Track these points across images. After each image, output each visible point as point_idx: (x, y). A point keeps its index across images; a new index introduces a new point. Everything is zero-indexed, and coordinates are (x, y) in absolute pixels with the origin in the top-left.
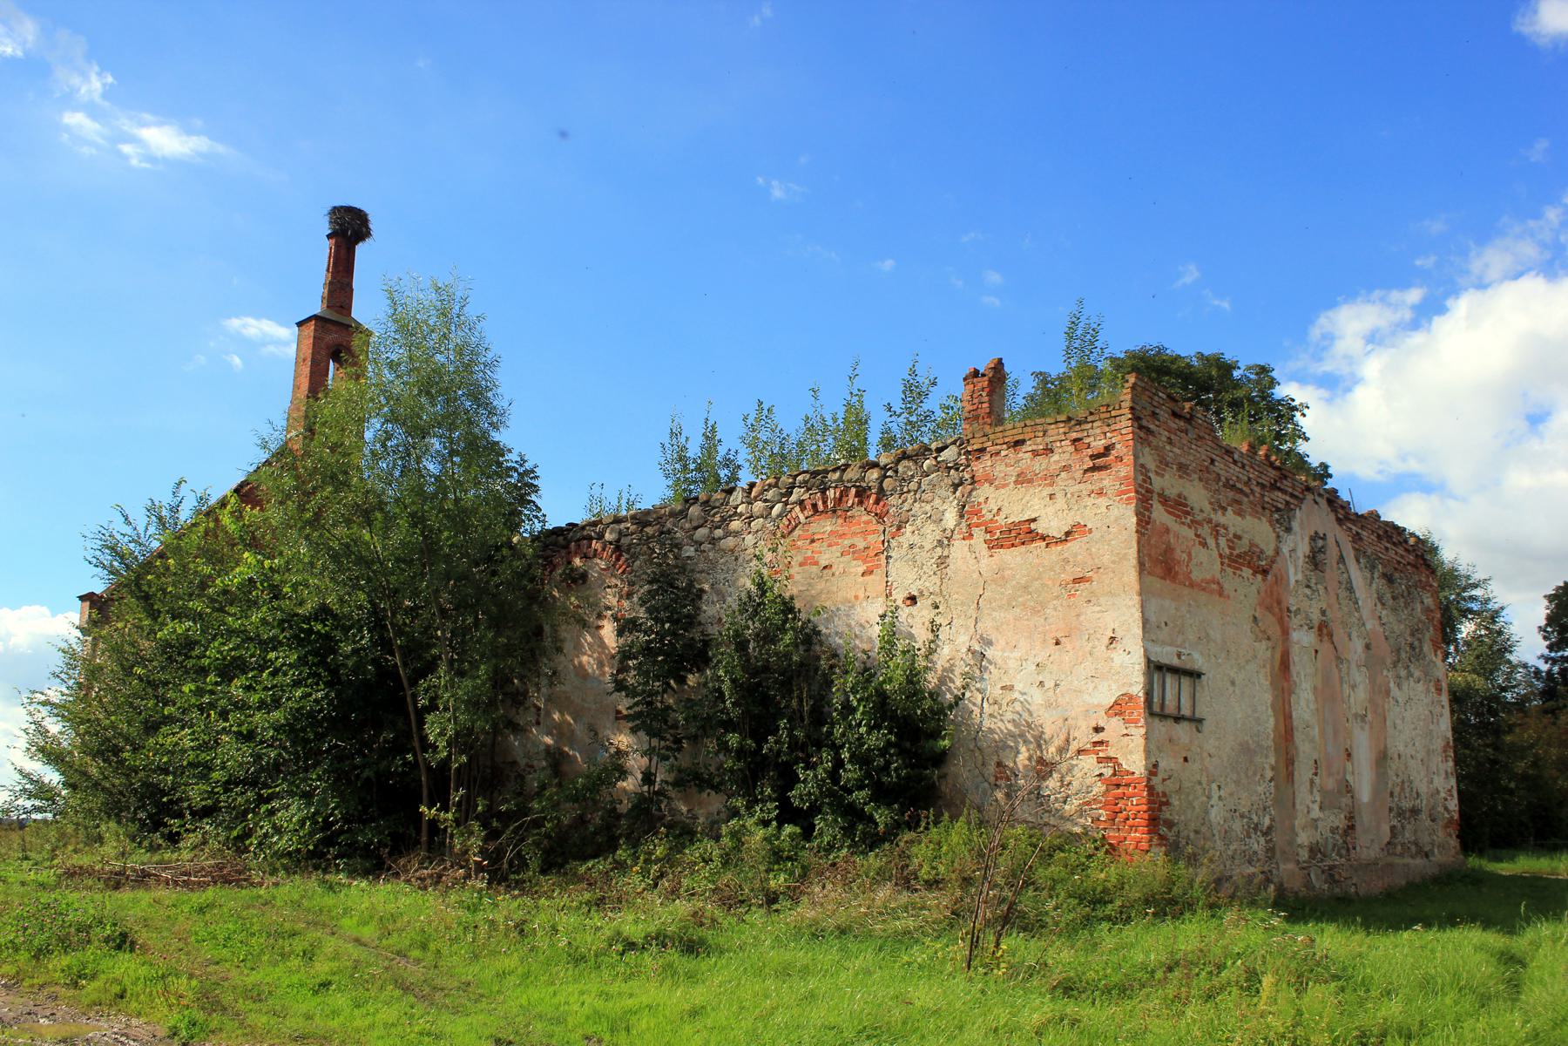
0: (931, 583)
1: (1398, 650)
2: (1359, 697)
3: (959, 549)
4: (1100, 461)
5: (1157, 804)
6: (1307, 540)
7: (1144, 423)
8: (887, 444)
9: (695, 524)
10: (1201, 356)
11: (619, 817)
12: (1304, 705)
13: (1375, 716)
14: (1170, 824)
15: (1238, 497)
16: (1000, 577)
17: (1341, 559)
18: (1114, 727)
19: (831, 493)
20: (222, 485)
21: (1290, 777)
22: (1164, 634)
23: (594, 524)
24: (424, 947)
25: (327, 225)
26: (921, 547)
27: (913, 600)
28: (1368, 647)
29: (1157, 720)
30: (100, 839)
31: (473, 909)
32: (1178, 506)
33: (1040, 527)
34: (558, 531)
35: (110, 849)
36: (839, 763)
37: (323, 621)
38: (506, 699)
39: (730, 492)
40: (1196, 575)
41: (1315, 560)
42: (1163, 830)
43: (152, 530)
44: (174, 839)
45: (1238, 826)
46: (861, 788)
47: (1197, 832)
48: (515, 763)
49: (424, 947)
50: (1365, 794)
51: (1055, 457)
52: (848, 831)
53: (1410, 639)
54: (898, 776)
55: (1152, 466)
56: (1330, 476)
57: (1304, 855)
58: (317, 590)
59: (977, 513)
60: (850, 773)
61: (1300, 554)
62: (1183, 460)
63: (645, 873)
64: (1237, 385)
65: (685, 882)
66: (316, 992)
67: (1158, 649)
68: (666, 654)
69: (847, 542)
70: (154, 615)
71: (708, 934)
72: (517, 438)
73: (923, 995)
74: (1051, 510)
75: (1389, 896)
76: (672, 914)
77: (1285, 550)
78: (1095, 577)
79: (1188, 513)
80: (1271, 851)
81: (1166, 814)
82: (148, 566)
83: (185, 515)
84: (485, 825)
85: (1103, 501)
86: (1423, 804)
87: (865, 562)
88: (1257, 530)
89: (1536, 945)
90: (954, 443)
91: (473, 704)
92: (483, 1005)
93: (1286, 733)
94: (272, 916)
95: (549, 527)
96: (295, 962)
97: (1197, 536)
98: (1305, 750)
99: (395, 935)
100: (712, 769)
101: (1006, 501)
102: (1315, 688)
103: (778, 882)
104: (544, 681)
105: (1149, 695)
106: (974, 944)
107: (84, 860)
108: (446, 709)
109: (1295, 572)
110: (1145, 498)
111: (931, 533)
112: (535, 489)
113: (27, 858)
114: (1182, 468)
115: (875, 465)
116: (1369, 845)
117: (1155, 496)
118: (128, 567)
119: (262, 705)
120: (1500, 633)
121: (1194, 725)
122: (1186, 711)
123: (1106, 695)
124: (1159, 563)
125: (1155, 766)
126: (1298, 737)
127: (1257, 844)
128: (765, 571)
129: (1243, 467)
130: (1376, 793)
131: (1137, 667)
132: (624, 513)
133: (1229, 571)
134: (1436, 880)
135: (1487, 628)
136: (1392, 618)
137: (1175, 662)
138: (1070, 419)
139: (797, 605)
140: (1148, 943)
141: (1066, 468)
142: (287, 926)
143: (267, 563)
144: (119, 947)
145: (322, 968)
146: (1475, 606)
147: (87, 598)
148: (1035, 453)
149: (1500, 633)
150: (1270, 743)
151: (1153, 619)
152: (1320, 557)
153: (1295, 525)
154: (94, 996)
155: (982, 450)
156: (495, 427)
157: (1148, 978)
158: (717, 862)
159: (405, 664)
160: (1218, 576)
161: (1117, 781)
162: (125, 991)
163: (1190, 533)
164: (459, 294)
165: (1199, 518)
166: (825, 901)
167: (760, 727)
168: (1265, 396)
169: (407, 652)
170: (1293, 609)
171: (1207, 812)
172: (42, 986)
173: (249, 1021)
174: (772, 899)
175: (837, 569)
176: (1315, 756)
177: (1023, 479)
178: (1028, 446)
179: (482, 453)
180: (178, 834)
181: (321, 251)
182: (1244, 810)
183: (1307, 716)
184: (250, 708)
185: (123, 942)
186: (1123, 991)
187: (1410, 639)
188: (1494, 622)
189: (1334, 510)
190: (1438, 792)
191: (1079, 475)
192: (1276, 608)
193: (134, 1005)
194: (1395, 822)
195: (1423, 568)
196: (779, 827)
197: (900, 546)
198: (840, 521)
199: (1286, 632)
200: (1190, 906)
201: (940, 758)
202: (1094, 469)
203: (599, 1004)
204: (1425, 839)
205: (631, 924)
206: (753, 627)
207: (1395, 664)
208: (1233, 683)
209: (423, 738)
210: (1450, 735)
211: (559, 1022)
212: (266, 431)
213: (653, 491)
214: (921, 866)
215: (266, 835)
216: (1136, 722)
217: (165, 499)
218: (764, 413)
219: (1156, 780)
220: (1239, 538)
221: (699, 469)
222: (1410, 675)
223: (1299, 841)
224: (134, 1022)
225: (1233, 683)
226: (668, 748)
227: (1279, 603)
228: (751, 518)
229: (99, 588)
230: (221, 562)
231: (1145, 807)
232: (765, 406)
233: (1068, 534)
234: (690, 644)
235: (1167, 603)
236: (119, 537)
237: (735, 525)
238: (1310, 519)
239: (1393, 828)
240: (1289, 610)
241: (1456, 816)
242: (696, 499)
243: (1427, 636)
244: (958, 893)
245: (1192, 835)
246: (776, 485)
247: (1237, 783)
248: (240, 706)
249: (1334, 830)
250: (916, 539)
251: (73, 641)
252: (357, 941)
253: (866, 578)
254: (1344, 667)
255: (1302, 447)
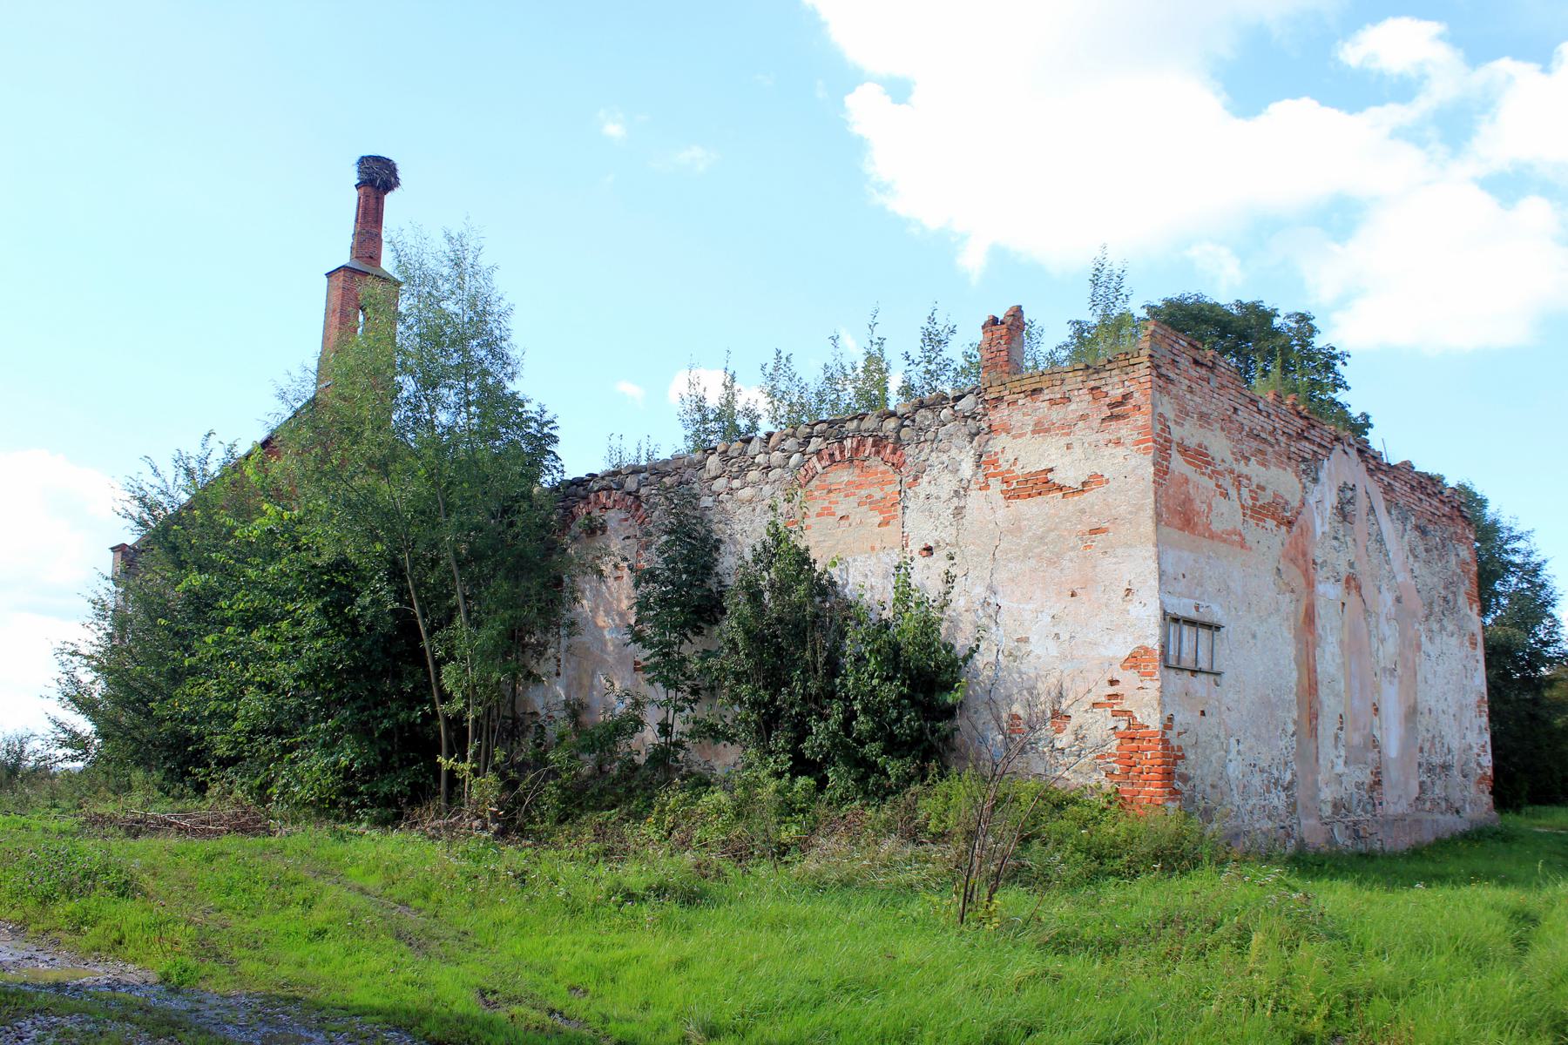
0: (948, 535)
1: (1431, 604)
2: (1388, 650)
3: (975, 499)
4: (1118, 410)
5: (1172, 758)
6: (1335, 491)
7: (1163, 371)
8: (907, 390)
9: (713, 474)
10: (1240, 304)
11: (636, 768)
12: (1329, 659)
13: (1406, 669)
14: (1185, 779)
15: (1262, 447)
16: (1016, 528)
17: (1372, 509)
18: (1129, 679)
19: (848, 443)
20: (248, 437)
21: (1314, 732)
22: (1181, 586)
23: (615, 474)
24: (426, 897)
25: (356, 175)
26: (938, 498)
27: (929, 550)
28: (1398, 600)
29: (1172, 672)
30: (129, 787)
31: (477, 859)
32: (1199, 457)
33: (1055, 478)
34: (578, 482)
35: (137, 798)
36: (850, 716)
37: (343, 573)
38: (516, 647)
39: (748, 441)
40: (1217, 527)
41: (1343, 512)
42: (1178, 785)
43: (180, 481)
44: (201, 788)
45: (1257, 781)
46: (874, 740)
47: (1213, 786)
48: (535, 714)
49: (426, 897)
50: (1392, 748)
51: (1073, 406)
52: (861, 780)
53: (1443, 593)
54: (911, 728)
55: (1170, 415)
56: (1370, 426)
57: (1327, 810)
58: (329, 541)
59: (994, 463)
60: (863, 724)
61: (1328, 505)
62: (1204, 409)
63: (659, 822)
64: (1276, 333)
65: (697, 833)
66: (311, 940)
67: (1174, 601)
68: (683, 605)
69: (864, 492)
70: (181, 565)
71: (712, 885)
72: (536, 385)
73: (909, 950)
74: (1067, 460)
75: (1416, 853)
76: (677, 866)
77: (1311, 500)
78: (1112, 528)
79: (1208, 463)
80: (1292, 807)
81: (1181, 768)
82: (176, 518)
83: (214, 468)
84: (503, 776)
85: (1120, 451)
86: (1455, 760)
87: (881, 513)
88: (1282, 481)
89: (1550, 904)
90: (971, 392)
91: (487, 656)
92: (477, 954)
93: (1310, 688)
94: (277, 865)
95: (569, 476)
96: (295, 910)
97: (1218, 486)
98: (1330, 705)
99: (399, 884)
100: (728, 721)
101: (1023, 452)
102: (1341, 642)
103: (789, 833)
104: (563, 632)
105: (1164, 647)
106: (968, 898)
107: (108, 808)
108: (463, 659)
109: (1321, 522)
110: (1163, 447)
111: (948, 484)
112: (555, 440)
113: (55, 806)
114: (1203, 416)
115: (893, 414)
116: (1397, 799)
117: (1174, 446)
118: (155, 518)
119: (283, 655)
120: (1543, 586)
121: (1212, 677)
122: (1204, 665)
123: (1122, 648)
124: (1177, 515)
125: (1171, 719)
126: (1323, 691)
127: (1278, 800)
128: (781, 522)
129: (1269, 416)
130: (1405, 747)
131: (1153, 619)
132: (643, 463)
133: (1252, 522)
134: (1465, 836)
135: (1529, 582)
136: (1425, 571)
137: (1193, 615)
138: (1088, 367)
139: (813, 555)
140: (1149, 897)
141: (1083, 417)
142: (291, 874)
143: (286, 515)
144: (122, 895)
145: (319, 917)
146: (1517, 559)
147: (120, 549)
148: (1052, 402)
149: (1543, 586)
150: (1293, 697)
151: (1170, 570)
152: (1348, 508)
153: (1322, 475)
154: (93, 942)
155: (1000, 399)
156: (512, 377)
157: (1145, 934)
158: (730, 814)
159: (424, 615)
160: (1239, 527)
161: (1132, 735)
162: (123, 937)
163: (1211, 484)
164: (472, 244)
165: (1219, 468)
166: (829, 854)
167: (776, 680)
168: (1305, 345)
169: (426, 605)
170: (1319, 561)
171: (1225, 767)
172: (47, 932)
173: (239, 969)
174: (783, 850)
175: (855, 519)
176: (1341, 711)
177: (1040, 429)
178: (1046, 395)
179: (499, 406)
180: (204, 783)
181: (348, 200)
182: (1264, 765)
183: (1332, 670)
184: (271, 658)
185: (126, 889)
186: (1108, 948)
187: (1443, 593)
188: (1537, 575)
189: (1365, 460)
190: (1471, 748)
191: (1096, 424)
192: (1303, 562)
193: (131, 951)
194: (1424, 778)
195: (1459, 520)
196: (792, 780)
197: (916, 495)
198: (857, 471)
199: (1310, 585)
200: (1196, 863)
201: (950, 712)
202: (1112, 417)
203: (590, 955)
204: (1456, 796)
205: (633, 875)
206: (768, 576)
207: (1427, 618)
208: (1254, 636)
209: (441, 689)
210: (1484, 689)
211: (548, 973)
212: (284, 382)
213: (669, 440)
214: (928, 819)
215: (287, 785)
216: (1150, 674)
217: (194, 450)
218: (782, 360)
219: (1171, 735)
220: (1263, 489)
221: (718, 418)
222: (1442, 628)
223: (1322, 796)
224: (130, 967)
225: (1254, 636)
226: (685, 699)
227: (1304, 554)
228: (768, 468)
229: (131, 540)
230: (245, 513)
231: (1159, 761)
232: (784, 355)
233: (1084, 484)
234: (709, 595)
235: (1185, 554)
236: (147, 488)
237: (753, 475)
238: (1340, 468)
239: (1422, 784)
240: (1314, 563)
241: (1490, 772)
242: (715, 449)
243: (1462, 589)
244: (963, 846)
245: (1208, 789)
246: (794, 435)
247: (1257, 737)
248: (262, 657)
249: (1359, 786)
250: (932, 490)
251: (102, 592)
252: (362, 890)
253: (883, 529)
254: (1373, 621)
255: (1341, 396)
